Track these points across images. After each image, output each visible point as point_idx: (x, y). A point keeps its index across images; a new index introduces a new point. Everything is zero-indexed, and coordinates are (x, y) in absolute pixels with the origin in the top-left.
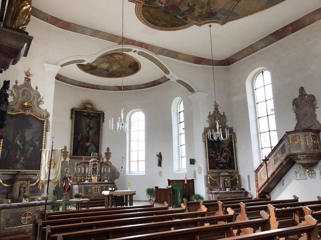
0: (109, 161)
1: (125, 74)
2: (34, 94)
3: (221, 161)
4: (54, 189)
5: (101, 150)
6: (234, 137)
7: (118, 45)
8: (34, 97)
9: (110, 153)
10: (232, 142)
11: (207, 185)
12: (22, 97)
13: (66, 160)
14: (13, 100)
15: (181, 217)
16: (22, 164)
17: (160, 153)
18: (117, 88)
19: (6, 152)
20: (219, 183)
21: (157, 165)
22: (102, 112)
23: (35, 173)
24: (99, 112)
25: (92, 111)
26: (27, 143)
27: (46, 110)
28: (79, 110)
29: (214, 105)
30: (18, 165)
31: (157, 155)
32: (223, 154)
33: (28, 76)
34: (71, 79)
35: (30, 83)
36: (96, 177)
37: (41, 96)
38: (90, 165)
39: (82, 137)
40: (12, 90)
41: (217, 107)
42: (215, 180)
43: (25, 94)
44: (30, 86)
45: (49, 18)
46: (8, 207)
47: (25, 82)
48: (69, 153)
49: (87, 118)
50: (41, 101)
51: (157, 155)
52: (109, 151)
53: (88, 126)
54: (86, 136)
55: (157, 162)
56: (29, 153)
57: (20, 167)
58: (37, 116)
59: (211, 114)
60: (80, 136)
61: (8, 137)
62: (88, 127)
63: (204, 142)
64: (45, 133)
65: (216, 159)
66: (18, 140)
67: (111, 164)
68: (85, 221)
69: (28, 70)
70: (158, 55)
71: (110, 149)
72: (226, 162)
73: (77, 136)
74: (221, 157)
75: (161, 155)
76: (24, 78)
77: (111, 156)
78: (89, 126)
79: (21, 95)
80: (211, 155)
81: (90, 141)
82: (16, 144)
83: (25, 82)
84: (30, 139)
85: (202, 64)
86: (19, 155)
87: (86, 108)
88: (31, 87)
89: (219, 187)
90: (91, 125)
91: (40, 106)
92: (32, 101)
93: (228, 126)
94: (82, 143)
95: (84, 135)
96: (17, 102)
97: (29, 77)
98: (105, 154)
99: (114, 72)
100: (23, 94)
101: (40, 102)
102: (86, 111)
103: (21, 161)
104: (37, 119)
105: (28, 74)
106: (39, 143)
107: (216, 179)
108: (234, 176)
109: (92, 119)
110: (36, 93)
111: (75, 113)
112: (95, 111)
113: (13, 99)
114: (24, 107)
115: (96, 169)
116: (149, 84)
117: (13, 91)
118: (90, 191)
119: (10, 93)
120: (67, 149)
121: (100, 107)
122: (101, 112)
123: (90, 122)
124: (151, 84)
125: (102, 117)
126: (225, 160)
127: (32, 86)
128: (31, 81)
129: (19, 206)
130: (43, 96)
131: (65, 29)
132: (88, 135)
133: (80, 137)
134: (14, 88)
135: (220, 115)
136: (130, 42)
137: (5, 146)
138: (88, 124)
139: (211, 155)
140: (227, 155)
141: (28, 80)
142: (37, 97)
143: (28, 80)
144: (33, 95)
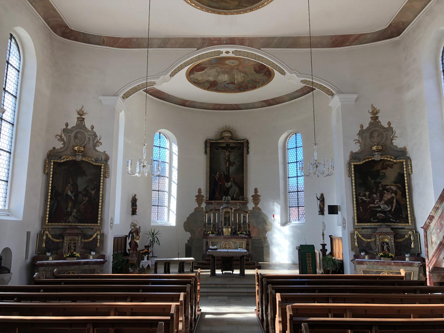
0: (258, 206)
1: (259, 82)
2: (89, 135)
3: (380, 208)
4: (187, 243)
6: (407, 165)
7: (197, 50)
8: (89, 138)
10: (404, 174)
11: (353, 248)
12: (75, 141)
13: (201, 206)
14: (62, 146)
15: (173, 298)
16: (74, 217)
17: (322, 195)
18: (264, 104)
19: (56, 204)
20: (375, 246)
21: (318, 213)
22: (245, 140)
23: (91, 227)
24: (241, 140)
25: (231, 141)
26: (80, 193)
27: (105, 152)
29: (370, 113)
30: (71, 219)
31: (318, 198)
32: (385, 195)
33: (81, 115)
34: (201, 103)
35: (84, 123)
36: (230, 230)
37: (97, 137)
38: (221, 213)
39: (220, 175)
40: (61, 134)
41: (377, 115)
42: (369, 240)
43: (78, 137)
44: (84, 126)
45: (105, 39)
46: (46, 265)
47: (78, 123)
48: (205, 197)
49: (225, 151)
50: (98, 142)
51: (318, 198)
52: (258, 194)
53: (227, 161)
54: (225, 174)
55: (317, 209)
56: (84, 205)
57: (73, 220)
58: (90, 161)
59: (365, 128)
60: (217, 174)
61: (56, 187)
62: (228, 163)
63: (349, 176)
64: (103, 180)
65: (371, 205)
66: (69, 190)
67: (261, 210)
68: (46, 290)
69: (82, 109)
70: (261, 49)
72: (390, 211)
73: (213, 175)
74: (380, 201)
75: (324, 197)
76: (77, 119)
77: (260, 199)
78: (229, 160)
79: (72, 139)
80: (361, 198)
81: (231, 181)
82: (67, 195)
83: (78, 123)
84: (84, 189)
85: (347, 44)
86: (70, 207)
87: (223, 138)
88: (86, 128)
89: (375, 252)
90: (232, 159)
91: (97, 148)
92: (86, 144)
93: (396, 146)
94: (220, 183)
95: (222, 173)
96: (68, 147)
97: (83, 117)
98: (252, 196)
99: (243, 83)
100: (76, 137)
101: (98, 143)
102: (223, 141)
103: (74, 213)
104: (92, 164)
105: (81, 114)
106: (95, 192)
107: (370, 238)
108: (405, 234)
109: (232, 152)
110: (91, 134)
111: (209, 146)
112: (235, 140)
113: (62, 145)
114: (75, 153)
115: (229, 217)
116: (305, 90)
117: (63, 135)
119: (59, 138)
120: (202, 192)
121: (242, 134)
122: (243, 140)
123: (229, 155)
124: (308, 89)
125: (245, 147)
126: (388, 206)
127: (86, 127)
128: (85, 120)
129: (59, 265)
130: (100, 136)
131: (127, 48)
133: (218, 176)
134: (63, 132)
135: (383, 128)
136: (216, 42)
137: (54, 198)
138: (227, 158)
139: (361, 198)
140: (393, 198)
141: (81, 120)
142: (93, 138)
143: (81, 119)
144: (87, 136)
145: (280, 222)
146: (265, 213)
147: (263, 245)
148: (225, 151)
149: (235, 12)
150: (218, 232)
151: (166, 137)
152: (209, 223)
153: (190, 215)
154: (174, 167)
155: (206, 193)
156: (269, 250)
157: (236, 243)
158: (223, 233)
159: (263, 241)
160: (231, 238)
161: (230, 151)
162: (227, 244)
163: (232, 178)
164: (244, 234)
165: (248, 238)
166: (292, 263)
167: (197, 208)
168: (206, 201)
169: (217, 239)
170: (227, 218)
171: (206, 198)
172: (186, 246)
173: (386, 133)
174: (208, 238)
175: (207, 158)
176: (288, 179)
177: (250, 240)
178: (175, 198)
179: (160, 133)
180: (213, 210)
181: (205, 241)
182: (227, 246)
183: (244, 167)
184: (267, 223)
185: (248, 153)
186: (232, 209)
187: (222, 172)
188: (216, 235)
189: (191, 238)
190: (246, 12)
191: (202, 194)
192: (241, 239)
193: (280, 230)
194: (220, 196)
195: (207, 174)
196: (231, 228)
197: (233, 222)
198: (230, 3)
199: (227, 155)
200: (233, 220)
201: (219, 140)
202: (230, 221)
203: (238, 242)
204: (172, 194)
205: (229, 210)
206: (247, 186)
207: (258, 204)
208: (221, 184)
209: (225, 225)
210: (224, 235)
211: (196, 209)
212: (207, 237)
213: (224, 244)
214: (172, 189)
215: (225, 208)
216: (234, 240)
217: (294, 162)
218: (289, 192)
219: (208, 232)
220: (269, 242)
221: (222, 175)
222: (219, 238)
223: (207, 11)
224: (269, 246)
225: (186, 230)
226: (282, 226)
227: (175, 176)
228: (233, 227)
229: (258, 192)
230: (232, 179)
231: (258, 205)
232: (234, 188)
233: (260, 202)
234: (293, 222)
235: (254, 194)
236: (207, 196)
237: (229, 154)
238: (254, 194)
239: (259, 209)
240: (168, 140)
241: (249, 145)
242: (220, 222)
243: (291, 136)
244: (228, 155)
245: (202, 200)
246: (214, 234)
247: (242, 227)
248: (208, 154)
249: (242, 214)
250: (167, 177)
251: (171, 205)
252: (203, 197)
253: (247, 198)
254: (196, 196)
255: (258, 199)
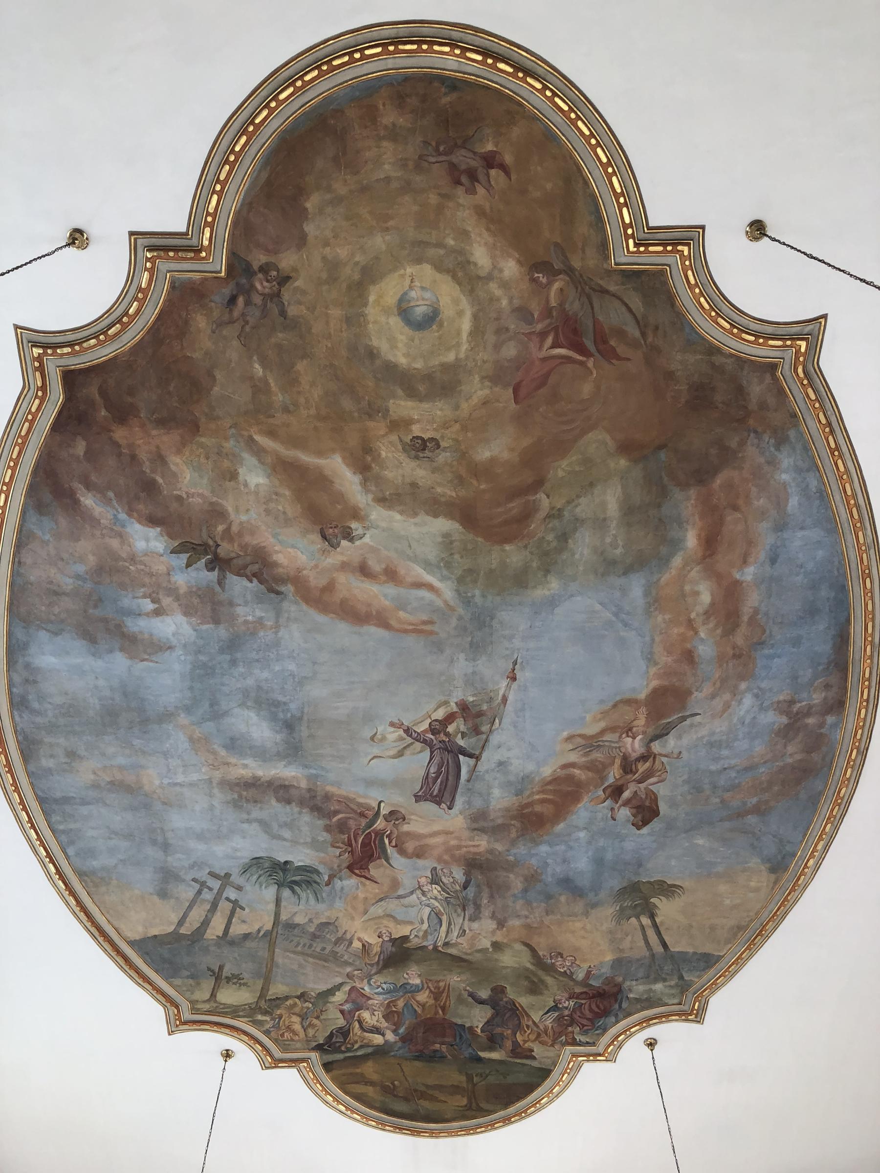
149: (462, 1129)
153: (436, 516)
173: (391, 299)
190: (491, 1126)
198: (445, 1102)
223: (381, 1125)
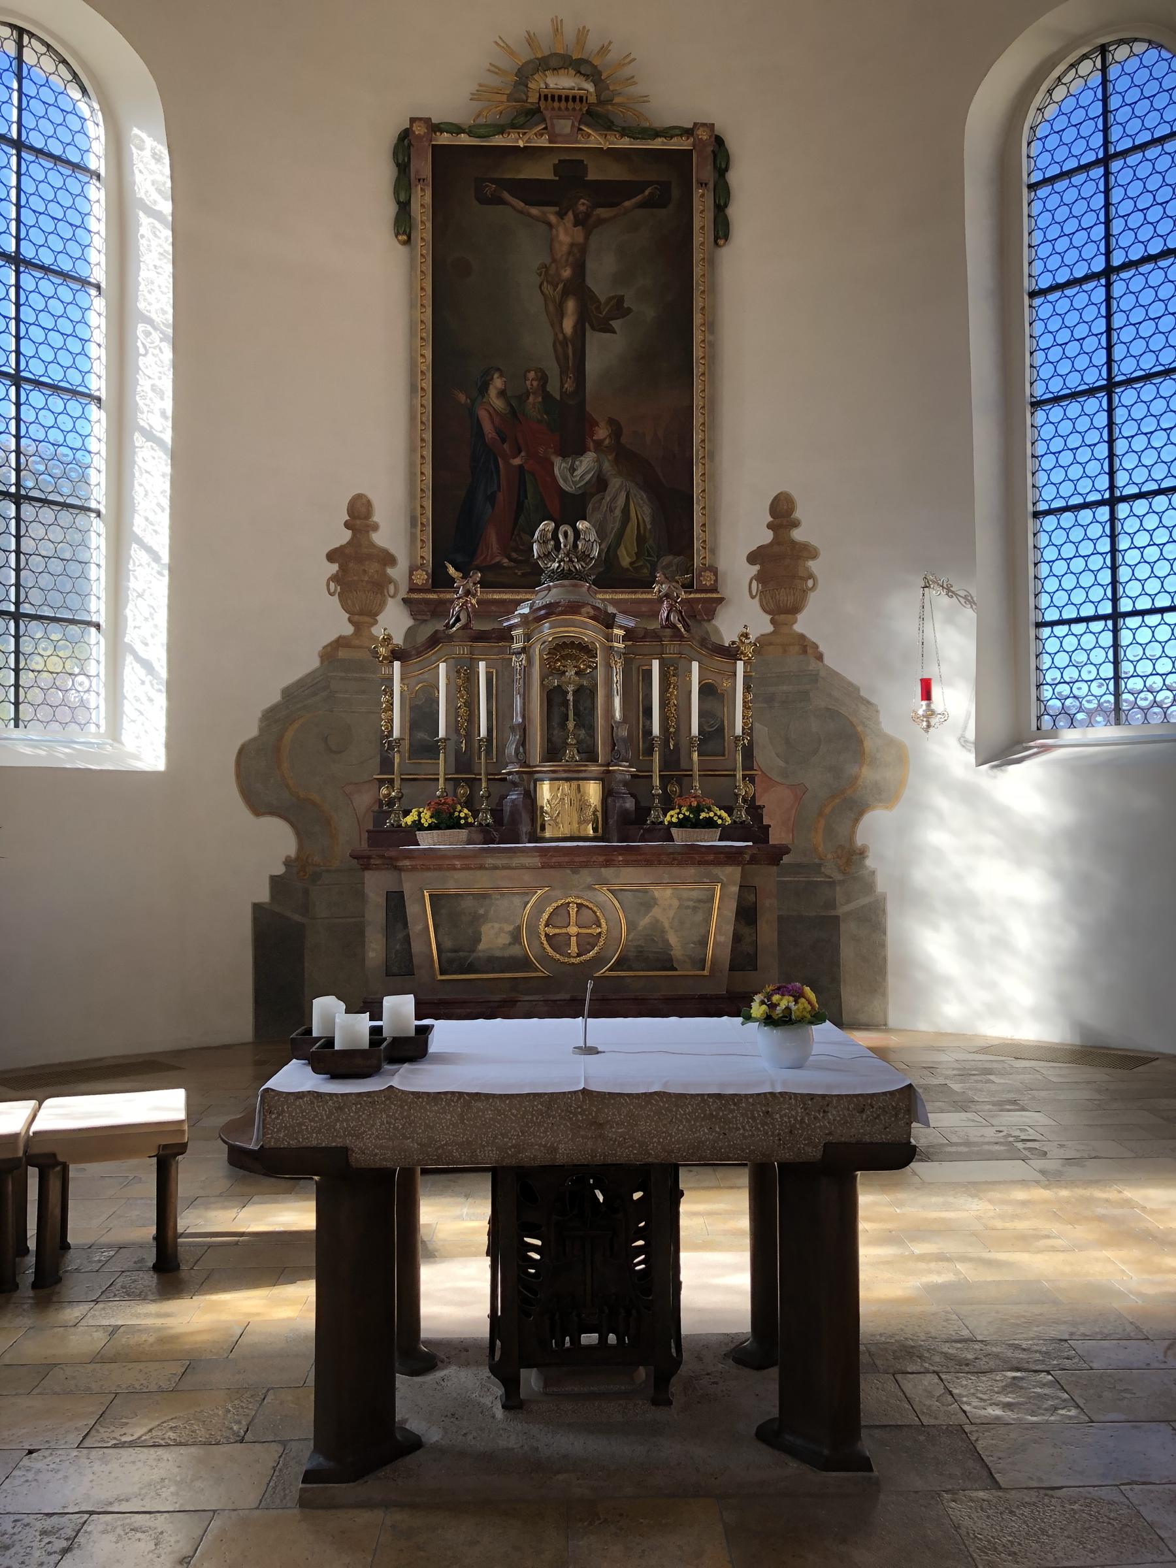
0: (798, 628)
4: (264, 896)
5: (715, 522)
9: (806, 552)
22: (703, 135)
25: (595, 140)
28: (470, 133)
36: (593, 792)
39: (515, 401)
49: (551, 214)
52: (797, 535)
53: (565, 294)
54: (553, 388)
60: (493, 392)
67: (820, 657)
71: (798, 514)
73: (462, 398)
77: (811, 576)
78: (577, 287)
81: (598, 444)
94: (517, 462)
98: (752, 558)
109: (601, 222)
111: (427, 172)
112: (625, 132)
115: (586, 694)
118: (504, 939)
120: (375, 528)
122: (688, 132)
125: (703, 184)
132: (569, 386)
133: (498, 404)
145: (971, 734)
146: (850, 678)
147: (831, 904)
148: (553, 219)
150: (497, 813)
151: (75, 76)
152: (426, 748)
153: (288, 693)
154: (150, 322)
155: (413, 537)
156: (883, 945)
157: (648, 904)
158: (533, 820)
159: (838, 877)
160: (608, 864)
161: (588, 215)
162: (573, 910)
163: (602, 424)
164: (716, 826)
165: (754, 860)
166: (1078, 1041)
167: (340, 643)
168: (411, 590)
169: (481, 867)
170: (570, 697)
171: (412, 570)
172: (256, 920)
174: (407, 863)
175: (412, 267)
176: (1028, 415)
177: (767, 878)
178: (156, 557)
179: (21, 31)
180: (450, 638)
181: (376, 885)
182: (573, 930)
183: (697, 336)
184: (869, 744)
185: (726, 237)
186: (608, 622)
187: (532, 375)
188: (480, 837)
189: (298, 858)
191: (380, 539)
192: (691, 871)
193: (970, 796)
194: (514, 555)
195: (413, 388)
196: (605, 779)
197: (623, 732)
199: (565, 249)
200: (618, 715)
201: (501, 130)
202: (591, 729)
203: (664, 895)
204: (139, 525)
205: (590, 633)
206: (710, 477)
207: (795, 609)
208: (521, 467)
209: (552, 753)
210: (547, 834)
211: (332, 653)
212: (392, 853)
213: (545, 916)
214: (138, 493)
215: (551, 610)
216: (630, 876)
217: (1079, 273)
218: (1036, 515)
219: (407, 813)
220: (881, 885)
221: (531, 399)
222: (499, 862)
224: (884, 911)
225: (257, 805)
226: (986, 767)
227: (154, 388)
228: (623, 770)
229: (796, 524)
230: (602, 433)
231: (800, 617)
232: (623, 495)
233: (812, 597)
234: (1070, 735)
235: (767, 537)
236: (419, 552)
237: (580, 239)
238: (767, 537)
239: (806, 647)
240: (96, 106)
241: (733, 177)
242: (513, 728)
243: (1059, 79)
244: (572, 245)
245: (380, 586)
246: (460, 827)
247: (696, 773)
248: (416, 235)
249: (695, 666)
250: (99, 400)
251: (129, 612)
252: (389, 559)
253: (714, 570)
254: (331, 557)
255: (802, 573)
